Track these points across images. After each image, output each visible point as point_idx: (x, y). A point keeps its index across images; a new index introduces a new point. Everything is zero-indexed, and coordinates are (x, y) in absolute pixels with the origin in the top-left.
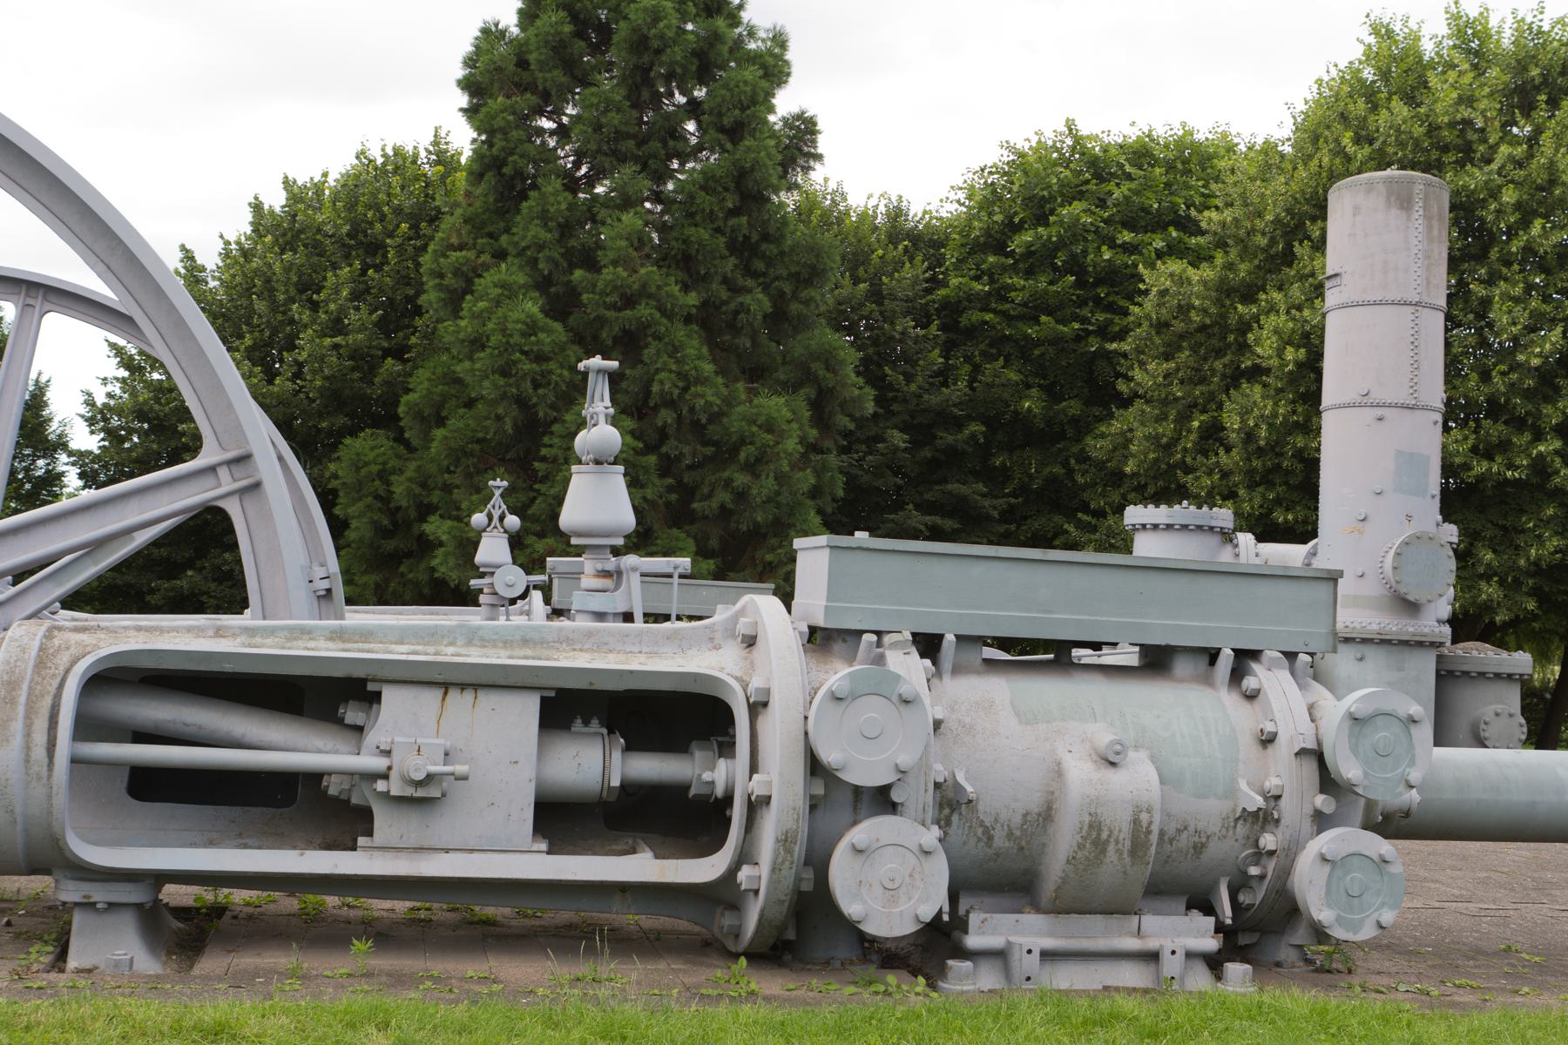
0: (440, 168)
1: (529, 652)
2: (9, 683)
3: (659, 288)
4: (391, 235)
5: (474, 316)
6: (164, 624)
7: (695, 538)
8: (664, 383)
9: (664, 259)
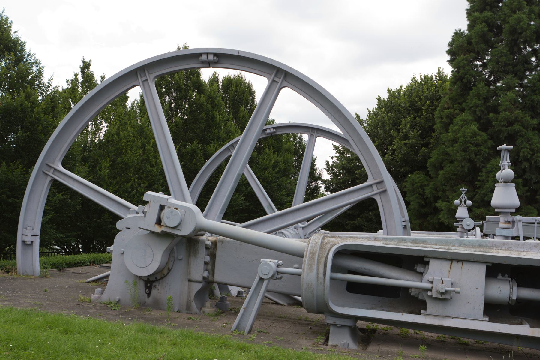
0: (440, 81)
1: (482, 250)
2: (312, 253)
3: (522, 118)
4: (423, 105)
5: (453, 132)
6: (358, 236)
7: (537, 209)
8: (525, 152)
9: (524, 108)
